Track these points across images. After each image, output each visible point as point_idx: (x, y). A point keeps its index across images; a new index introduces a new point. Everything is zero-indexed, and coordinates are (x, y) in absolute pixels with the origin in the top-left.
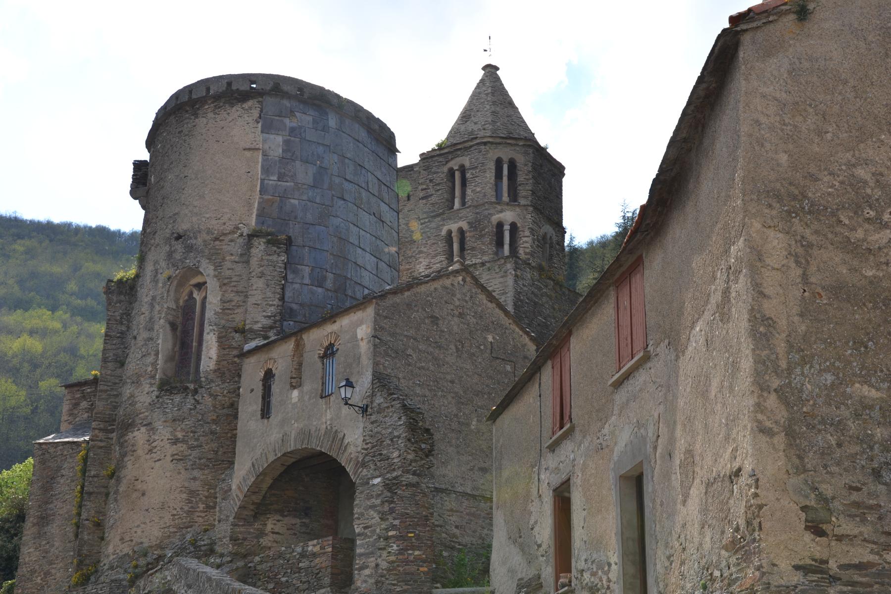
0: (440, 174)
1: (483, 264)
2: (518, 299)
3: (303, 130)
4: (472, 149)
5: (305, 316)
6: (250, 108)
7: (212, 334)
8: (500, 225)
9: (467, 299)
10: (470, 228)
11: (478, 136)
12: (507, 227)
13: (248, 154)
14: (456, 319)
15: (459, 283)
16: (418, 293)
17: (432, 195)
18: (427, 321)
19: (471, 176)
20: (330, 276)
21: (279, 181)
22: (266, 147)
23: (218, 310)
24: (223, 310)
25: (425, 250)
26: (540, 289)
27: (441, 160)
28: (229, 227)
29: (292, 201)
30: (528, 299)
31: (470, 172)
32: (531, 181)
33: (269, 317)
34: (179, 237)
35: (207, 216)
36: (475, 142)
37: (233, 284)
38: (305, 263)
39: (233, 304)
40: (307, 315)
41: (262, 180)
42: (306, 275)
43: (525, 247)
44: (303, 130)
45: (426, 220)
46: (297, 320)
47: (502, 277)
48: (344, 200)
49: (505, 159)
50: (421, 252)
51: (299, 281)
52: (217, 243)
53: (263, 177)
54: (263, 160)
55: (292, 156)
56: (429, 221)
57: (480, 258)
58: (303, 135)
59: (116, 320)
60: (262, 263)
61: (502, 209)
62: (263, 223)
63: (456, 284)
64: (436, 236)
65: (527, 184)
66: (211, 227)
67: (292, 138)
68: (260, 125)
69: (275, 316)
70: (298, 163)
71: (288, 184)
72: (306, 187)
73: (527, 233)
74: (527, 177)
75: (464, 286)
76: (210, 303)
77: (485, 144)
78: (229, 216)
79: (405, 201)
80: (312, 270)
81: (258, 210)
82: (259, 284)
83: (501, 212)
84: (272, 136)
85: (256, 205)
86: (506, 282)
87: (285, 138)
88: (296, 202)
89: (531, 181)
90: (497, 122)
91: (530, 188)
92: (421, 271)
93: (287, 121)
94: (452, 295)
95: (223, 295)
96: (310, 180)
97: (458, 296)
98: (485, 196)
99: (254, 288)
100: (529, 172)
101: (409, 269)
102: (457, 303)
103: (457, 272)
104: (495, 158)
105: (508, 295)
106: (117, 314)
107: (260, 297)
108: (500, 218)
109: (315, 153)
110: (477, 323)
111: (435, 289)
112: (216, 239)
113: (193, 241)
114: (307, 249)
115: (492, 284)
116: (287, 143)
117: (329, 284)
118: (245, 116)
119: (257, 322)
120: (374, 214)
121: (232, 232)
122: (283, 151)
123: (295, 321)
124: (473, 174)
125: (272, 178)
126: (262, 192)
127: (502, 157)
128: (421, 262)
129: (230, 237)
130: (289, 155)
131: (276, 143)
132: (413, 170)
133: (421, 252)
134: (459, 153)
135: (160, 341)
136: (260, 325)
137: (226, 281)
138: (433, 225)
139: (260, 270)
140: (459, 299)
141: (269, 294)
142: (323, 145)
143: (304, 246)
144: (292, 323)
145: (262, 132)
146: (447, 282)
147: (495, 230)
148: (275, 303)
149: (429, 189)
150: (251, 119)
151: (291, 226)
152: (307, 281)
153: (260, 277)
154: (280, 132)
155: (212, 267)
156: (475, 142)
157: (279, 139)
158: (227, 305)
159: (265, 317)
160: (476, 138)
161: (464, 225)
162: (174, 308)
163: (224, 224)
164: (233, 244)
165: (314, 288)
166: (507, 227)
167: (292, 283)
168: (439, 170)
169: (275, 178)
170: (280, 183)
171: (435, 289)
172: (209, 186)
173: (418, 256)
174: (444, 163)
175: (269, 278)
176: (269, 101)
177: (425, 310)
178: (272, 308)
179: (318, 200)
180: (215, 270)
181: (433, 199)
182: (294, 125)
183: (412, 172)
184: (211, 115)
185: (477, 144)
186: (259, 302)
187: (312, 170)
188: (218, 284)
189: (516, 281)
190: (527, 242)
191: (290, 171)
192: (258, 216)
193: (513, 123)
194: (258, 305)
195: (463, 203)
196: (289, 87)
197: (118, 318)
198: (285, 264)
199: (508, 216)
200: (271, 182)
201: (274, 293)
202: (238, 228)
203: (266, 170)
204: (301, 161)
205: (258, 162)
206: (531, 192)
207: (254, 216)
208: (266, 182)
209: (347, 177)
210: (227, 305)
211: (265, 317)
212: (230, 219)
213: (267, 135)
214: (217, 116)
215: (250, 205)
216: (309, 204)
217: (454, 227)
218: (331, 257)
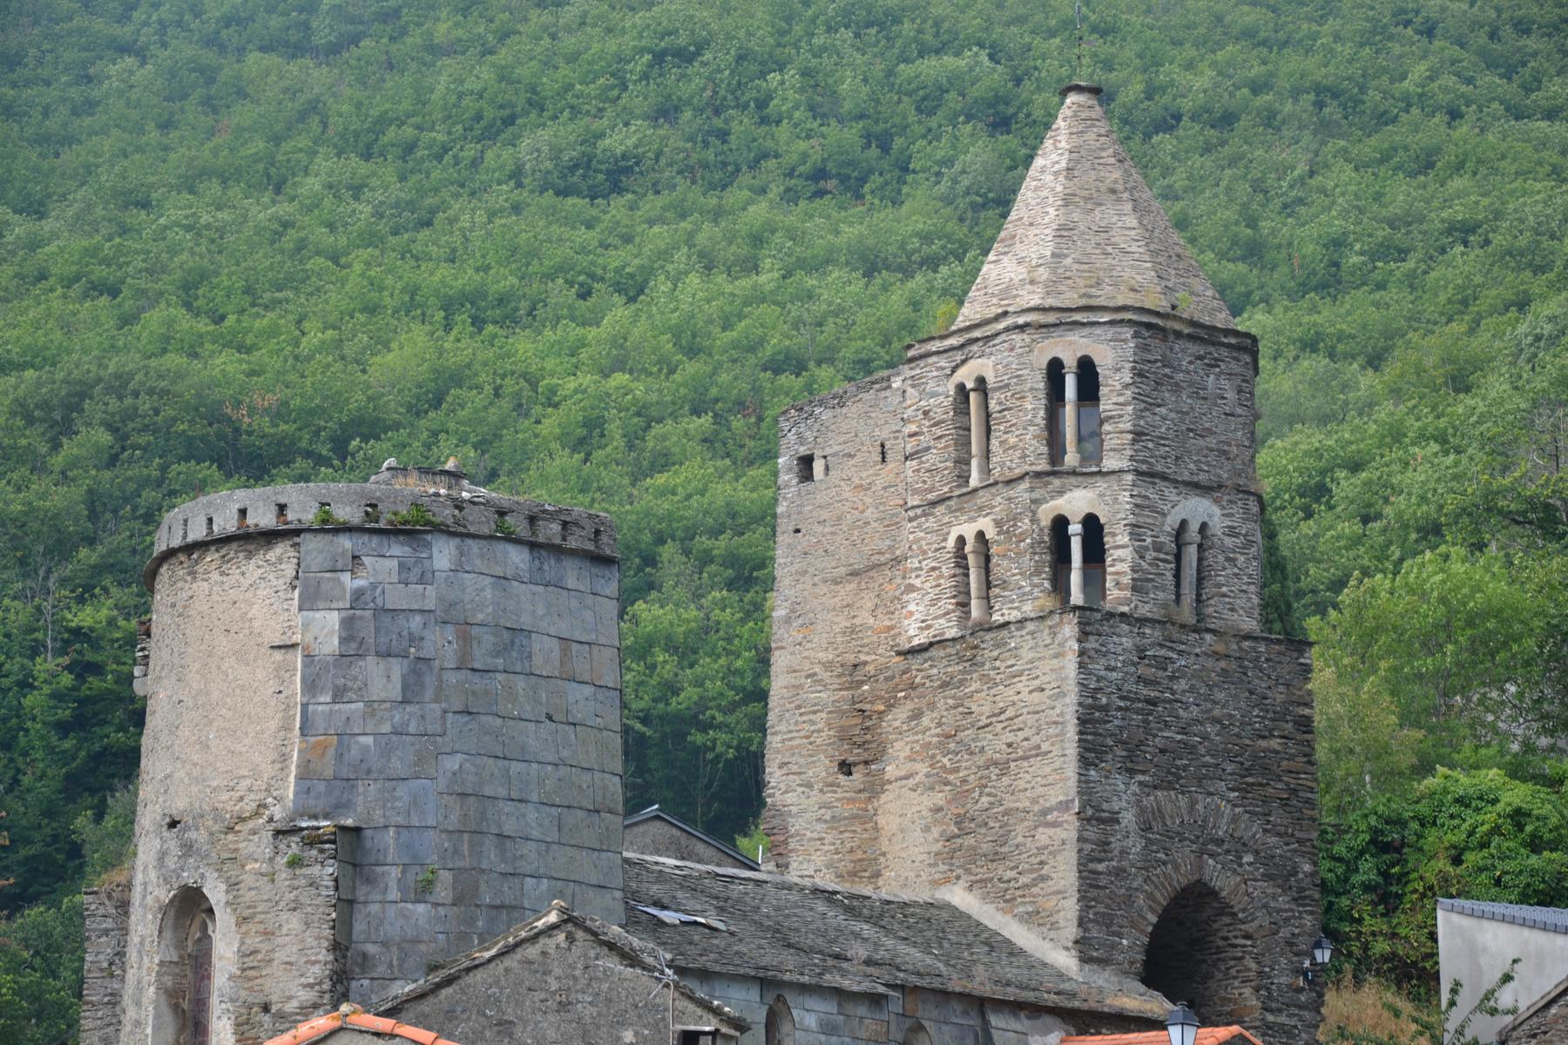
0: (941, 398)
1: (1021, 622)
2: (1091, 707)
3: (379, 590)
4: (996, 341)
5: (391, 966)
6: (280, 560)
7: (225, 1019)
8: (1060, 523)
9: (578, 973)
10: (999, 533)
11: (1010, 309)
12: (1075, 528)
13: (278, 656)
14: (552, 1018)
15: (558, 947)
16: (469, 986)
17: (928, 449)
18: (488, 1034)
19: (998, 408)
20: (446, 876)
21: (334, 702)
22: (309, 638)
23: (235, 970)
24: (244, 970)
25: (917, 583)
26: (1162, 663)
27: (943, 364)
28: (249, 806)
29: (362, 739)
30: (1122, 698)
31: (997, 395)
32: (1130, 408)
33: (311, 986)
34: (173, 824)
35: (214, 784)
36: (1001, 325)
37: (260, 917)
38: (389, 859)
39: (260, 957)
40: (395, 962)
41: (305, 706)
42: (393, 884)
43: (1117, 573)
44: (379, 590)
45: (919, 511)
46: (375, 975)
47: (1056, 656)
48: (470, 713)
49: (1070, 362)
50: (911, 588)
51: (379, 898)
52: (231, 837)
53: (305, 700)
54: (305, 665)
55: (360, 647)
56: (925, 514)
57: (1018, 608)
58: (379, 601)
59: (102, 970)
60: (296, 883)
61: (1063, 486)
62: (308, 791)
63: (552, 951)
64: (937, 550)
65: (1121, 416)
66: (220, 806)
67: (358, 612)
68: (297, 592)
69: (320, 983)
70: (371, 660)
71: (353, 706)
72: (388, 705)
73: (1123, 539)
74: (1121, 399)
75: (569, 949)
76: (221, 958)
77: (1022, 328)
78: (248, 782)
79: (876, 463)
80: (403, 872)
81: (298, 766)
82: (293, 922)
83: (1061, 493)
84: (319, 615)
85: (295, 758)
86: (1062, 668)
87: (344, 614)
88: (369, 740)
89: (1130, 408)
90: (1066, 256)
91: (1128, 426)
92: (911, 633)
93: (346, 577)
94: (544, 973)
95: (242, 943)
96: (395, 691)
97: (557, 971)
98: (1024, 456)
99: (284, 931)
100: (1126, 386)
101: (890, 628)
102: (554, 986)
103: (554, 927)
104: (1044, 363)
105: (1068, 700)
106: (102, 957)
107: (295, 949)
108: (1056, 508)
109: (405, 633)
110: (599, 1014)
111: (507, 970)
112: (230, 829)
113: (192, 835)
114: (392, 831)
115: (1038, 672)
116: (348, 624)
117: (443, 892)
118: (271, 577)
119: (290, 998)
120: (550, 718)
121: (256, 814)
122: (342, 641)
123: (372, 979)
124: (1000, 403)
125: (322, 699)
126: (304, 731)
127: (1060, 356)
128: (911, 613)
129: (251, 825)
130: (352, 648)
131: (326, 627)
132: (889, 387)
133: (911, 588)
134: (975, 348)
135: (149, 1031)
136: (295, 1003)
137: (247, 913)
138: (931, 523)
139: (292, 896)
140: (558, 978)
141: (311, 941)
142: (422, 611)
143: (386, 827)
144: (366, 982)
145: (300, 609)
146: (532, 951)
147: (1046, 539)
148: (321, 957)
149: (921, 433)
150: (281, 581)
151: (361, 789)
152: (394, 894)
153: (294, 909)
154: (335, 605)
155: (223, 887)
156: (1001, 325)
157: (333, 619)
158: (250, 961)
159: (304, 986)
160: (1005, 313)
161: (986, 524)
162: (175, 959)
163: (242, 799)
164: (256, 838)
165: (410, 906)
166: (1075, 528)
167: (366, 903)
168: (940, 390)
169: (328, 699)
170: (337, 707)
171: (507, 970)
172: (216, 724)
173: (905, 597)
174: (948, 371)
175: (309, 909)
176: (311, 543)
177: (484, 1015)
178: (316, 969)
179: (412, 729)
180: (227, 892)
181: (931, 458)
182: (361, 583)
183: (888, 393)
184: (215, 576)
185: (1007, 330)
186: (292, 959)
187: (397, 668)
188: (233, 920)
189: (1081, 665)
190: (1122, 561)
191: (355, 679)
192: (300, 778)
193: (1109, 249)
194: (290, 964)
195: (986, 470)
196: (348, 509)
197: (105, 965)
198: (336, 880)
199: (1076, 502)
200: (320, 708)
201: (318, 938)
202: (265, 806)
203: (310, 686)
204: (378, 654)
205: (295, 669)
206: (1130, 436)
207: (292, 779)
208: (311, 708)
209: (477, 665)
210: (250, 961)
211: (304, 986)
212: (250, 790)
213: (311, 614)
214: (225, 579)
215: (284, 758)
216: (394, 738)
217: (969, 531)
218: (444, 836)
